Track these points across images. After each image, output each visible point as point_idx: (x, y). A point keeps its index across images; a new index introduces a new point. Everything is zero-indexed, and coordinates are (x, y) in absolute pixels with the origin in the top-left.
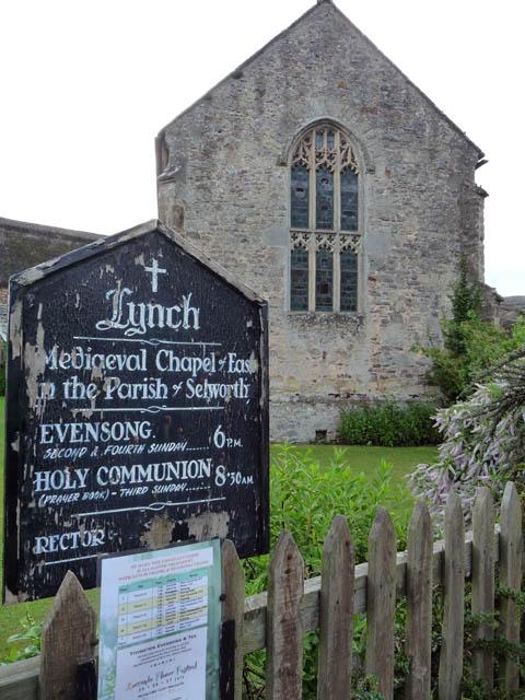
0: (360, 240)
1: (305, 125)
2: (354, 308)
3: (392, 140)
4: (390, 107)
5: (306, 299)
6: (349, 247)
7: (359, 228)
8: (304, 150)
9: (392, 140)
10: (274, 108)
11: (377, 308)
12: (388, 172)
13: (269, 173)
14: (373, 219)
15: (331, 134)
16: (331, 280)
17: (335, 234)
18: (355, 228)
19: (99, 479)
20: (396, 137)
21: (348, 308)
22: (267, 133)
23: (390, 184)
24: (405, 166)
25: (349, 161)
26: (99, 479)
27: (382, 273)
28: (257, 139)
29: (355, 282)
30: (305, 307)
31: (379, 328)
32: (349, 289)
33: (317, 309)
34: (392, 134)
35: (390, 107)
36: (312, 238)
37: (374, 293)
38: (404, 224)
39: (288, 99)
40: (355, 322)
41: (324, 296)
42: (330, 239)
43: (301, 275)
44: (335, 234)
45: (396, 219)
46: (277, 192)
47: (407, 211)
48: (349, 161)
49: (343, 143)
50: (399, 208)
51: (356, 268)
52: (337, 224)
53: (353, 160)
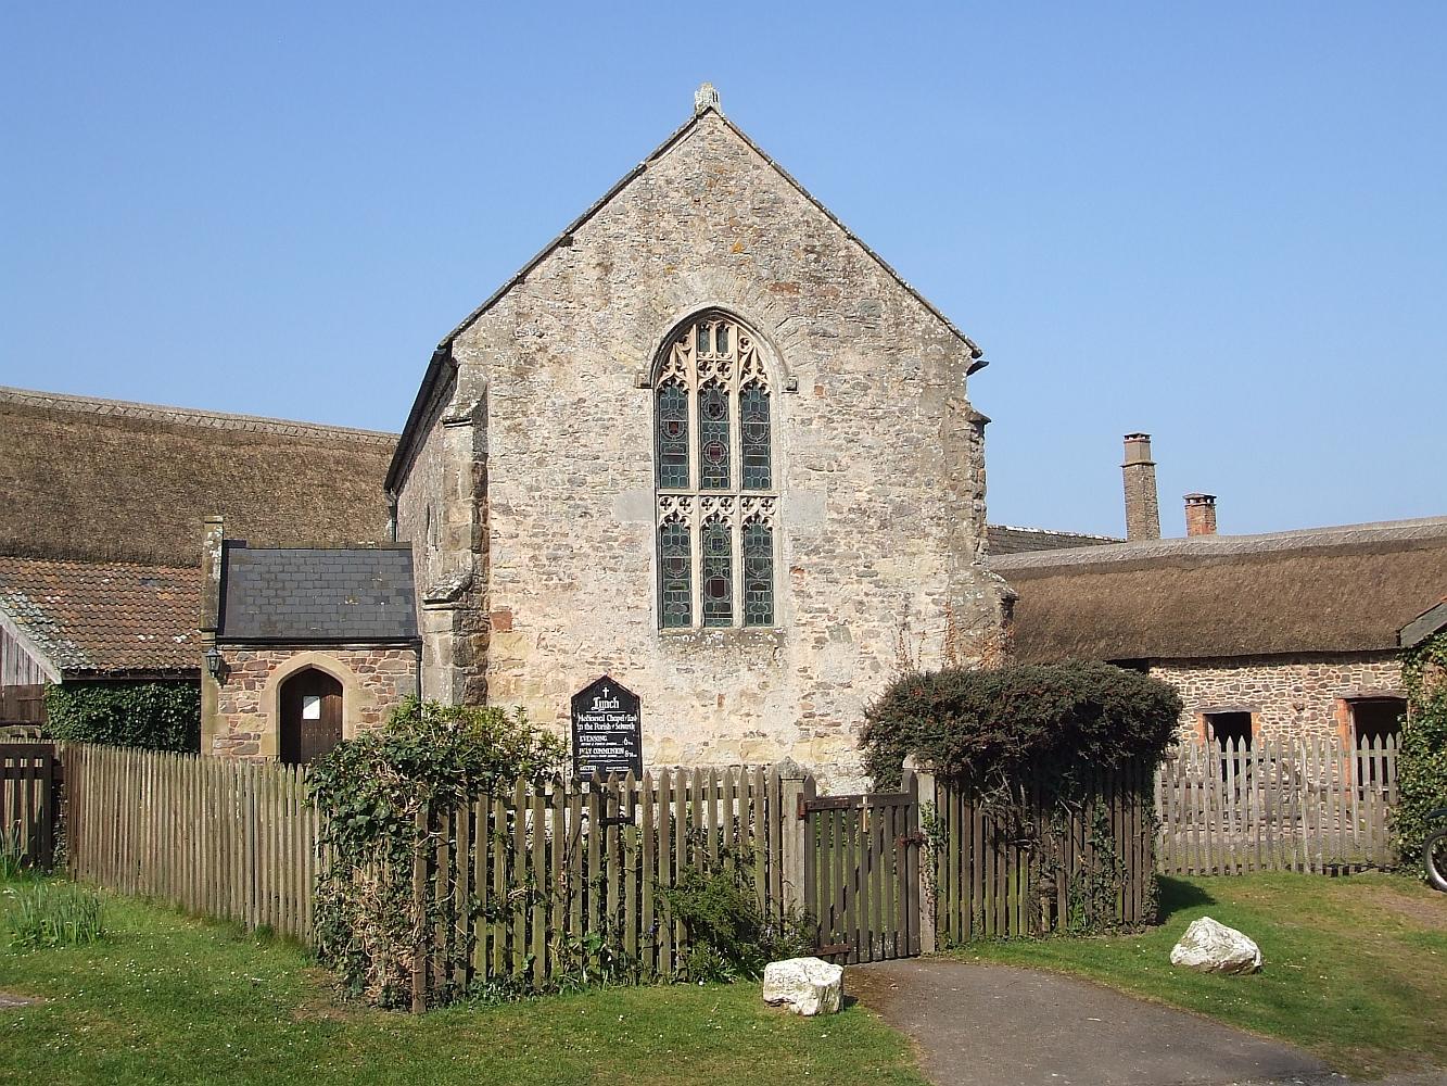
2: (769, 620)
4: (819, 281)
5: (689, 607)
7: (774, 484)
13: (622, 399)
14: (798, 470)
16: (729, 574)
18: (766, 484)
20: (831, 330)
21: (759, 620)
23: (824, 410)
24: (847, 377)
27: (815, 559)
29: (769, 575)
30: (687, 620)
31: (810, 649)
34: (824, 324)
35: (819, 281)
36: (695, 503)
37: (799, 593)
38: (849, 473)
40: (771, 642)
46: (635, 432)
47: (853, 452)
49: (744, 343)
50: (839, 448)
53: (760, 371)
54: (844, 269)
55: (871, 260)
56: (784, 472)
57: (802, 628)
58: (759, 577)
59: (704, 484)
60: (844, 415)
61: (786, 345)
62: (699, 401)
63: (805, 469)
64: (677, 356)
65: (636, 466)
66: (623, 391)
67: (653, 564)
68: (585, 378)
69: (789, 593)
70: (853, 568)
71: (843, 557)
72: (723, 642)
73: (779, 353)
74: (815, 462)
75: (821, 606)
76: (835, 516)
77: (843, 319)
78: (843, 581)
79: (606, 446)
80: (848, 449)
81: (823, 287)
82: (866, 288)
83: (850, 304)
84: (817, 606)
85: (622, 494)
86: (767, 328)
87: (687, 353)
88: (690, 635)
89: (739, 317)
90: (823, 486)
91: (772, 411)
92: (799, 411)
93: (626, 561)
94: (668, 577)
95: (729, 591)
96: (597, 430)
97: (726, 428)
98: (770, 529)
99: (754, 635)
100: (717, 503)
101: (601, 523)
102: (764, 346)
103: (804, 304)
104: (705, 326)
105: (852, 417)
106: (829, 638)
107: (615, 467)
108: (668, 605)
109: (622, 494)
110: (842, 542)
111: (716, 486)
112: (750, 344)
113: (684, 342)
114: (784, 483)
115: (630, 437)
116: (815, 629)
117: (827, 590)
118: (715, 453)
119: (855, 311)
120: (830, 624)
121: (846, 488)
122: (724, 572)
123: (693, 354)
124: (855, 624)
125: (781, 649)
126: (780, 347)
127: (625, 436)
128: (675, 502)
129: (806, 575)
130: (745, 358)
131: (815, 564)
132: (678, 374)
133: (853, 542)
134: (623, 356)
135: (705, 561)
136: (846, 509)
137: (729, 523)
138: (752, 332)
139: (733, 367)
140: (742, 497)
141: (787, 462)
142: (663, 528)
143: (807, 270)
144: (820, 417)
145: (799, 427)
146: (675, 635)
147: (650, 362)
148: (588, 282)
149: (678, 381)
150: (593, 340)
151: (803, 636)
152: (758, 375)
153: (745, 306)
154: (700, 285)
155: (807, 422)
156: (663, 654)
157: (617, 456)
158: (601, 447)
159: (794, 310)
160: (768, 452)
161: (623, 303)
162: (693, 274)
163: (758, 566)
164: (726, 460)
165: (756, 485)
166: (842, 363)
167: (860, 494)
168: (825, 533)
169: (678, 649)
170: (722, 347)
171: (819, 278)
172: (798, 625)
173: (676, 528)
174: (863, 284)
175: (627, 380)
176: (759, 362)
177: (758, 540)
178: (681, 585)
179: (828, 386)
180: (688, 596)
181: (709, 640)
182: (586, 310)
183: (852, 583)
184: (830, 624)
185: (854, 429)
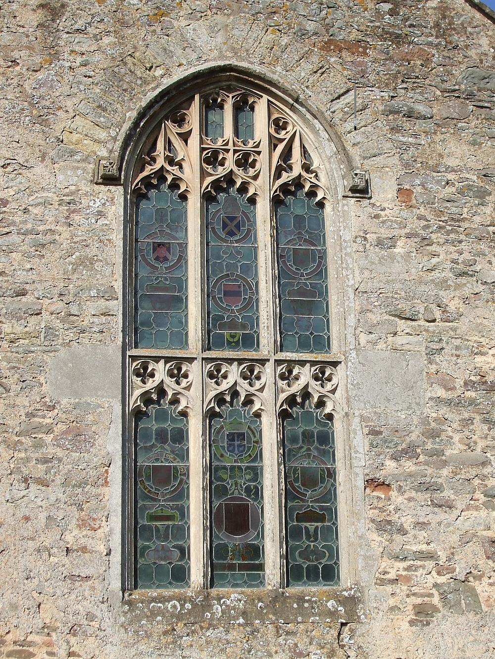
0: (339, 375)
1: (167, 82)
2: (330, 574)
3: (410, 115)
4: (398, 39)
5: (184, 552)
6: (235, 394)
7: (334, 343)
8: (169, 144)
9: (410, 115)
10: (87, 45)
11: (397, 568)
12: (404, 194)
13: (71, 203)
14: (373, 318)
15: (242, 107)
16: (256, 493)
17: (263, 362)
18: (323, 343)
19: (438, 187)
20: (421, 108)
21: (313, 575)
22: (69, 103)
23: (414, 225)
24: (451, 176)
25: (297, 170)
26: (438, 187)
27: (409, 466)
28: (42, 120)
29: (330, 496)
30: (180, 575)
31: (405, 625)
32: (311, 516)
33: (212, 582)
34: (408, 99)
35: (398, 39)
36: (195, 371)
37: (384, 526)
38: (463, 325)
39: (124, 24)
40: (333, 614)
41: (238, 540)
42: (249, 375)
43: (166, 481)
44: (263, 362)
45: (438, 314)
46: (92, 251)
47: (467, 291)
48: (297, 170)
49: (279, 125)
50: (443, 284)
51: (330, 455)
52: (267, 335)
53: (307, 168)
54: (437, 25)
55: (478, 15)
56: (352, 320)
57: (389, 589)
58: (310, 499)
59: (210, 341)
60: (448, 233)
61: (349, 126)
62: (282, 429)
63: (387, 317)
64: (169, 143)
65: (92, 307)
66: (73, 188)
67: (116, 473)
68: (10, 169)
69: (363, 526)
70: (477, 482)
71: (460, 464)
72: (244, 614)
73: (337, 138)
74: (402, 305)
75: (424, 547)
76: (441, 393)
77: (438, 93)
78: (459, 505)
79: (39, 274)
80: (458, 287)
81: (406, 48)
82: (472, 53)
83: (450, 73)
84: (415, 548)
85: (63, 353)
86: (317, 100)
87: (185, 137)
88: (182, 600)
89: (278, 88)
90: (418, 344)
91: (329, 228)
92: (372, 225)
93: (65, 468)
94: (146, 497)
95: (259, 524)
96: (25, 248)
97: (253, 254)
98: (330, 417)
99: (301, 599)
100: (234, 373)
101: (23, 401)
102: (316, 132)
103: (375, 71)
104: (215, 100)
105: (462, 237)
106: (439, 605)
107: (53, 308)
108: (145, 548)
109: (63, 353)
110: (457, 437)
111: (233, 344)
112: (289, 128)
113: (180, 121)
114: (351, 339)
115: (81, 262)
116: (415, 589)
117: (434, 519)
118: (232, 294)
119: (457, 84)
120: (441, 580)
121: (457, 348)
122: (248, 490)
123: (194, 140)
124: (485, 580)
125: (352, 625)
126: (341, 129)
127: (72, 259)
128: (160, 371)
129: (394, 494)
130: (281, 147)
131: (410, 475)
132: (169, 168)
133: (475, 438)
134: (75, 137)
135: (213, 471)
136: (459, 383)
137: (257, 406)
138: (292, 108)
139: (262, 161)
140: (278, 362)
141: (354, 304)
142: (138, 414)
143: (378, 24)
144: (408, 236)
145: (375, 253)
146: (154, 600)
147: (119, 144)
148: (21, 30)
149: (170, 178)
150: (26, 112)
151: (392, 602)
152: (304, 174)
153: (279, 69)
154: (205, 38)
155: (389, 243)
156: (130, 637)
157: (56, 291)
158: (32, 276)
159: (359, 81)
160: (323, 292)
161: (79, 60)
162: (195, 24)
163: (310, 479)
164: (252, 303)
165: (304, 345)
166: (441, 155)
167: (483, 358)
168: (425, 421)
169: (159, 626)
170: (242, 128)
171: (398, 36)
172: (382, 582)
173: (162, 416)
174: (467, 46)
175: (79, 172)
176: (304, 152)
177: (308, 436)
178: (170, 512)
179: (419, 189)
180: (182, 532)
181: (218, 609)
182: (18, 68)
183: (477, 508)
184: (441, 580)
185: (466, 256)
